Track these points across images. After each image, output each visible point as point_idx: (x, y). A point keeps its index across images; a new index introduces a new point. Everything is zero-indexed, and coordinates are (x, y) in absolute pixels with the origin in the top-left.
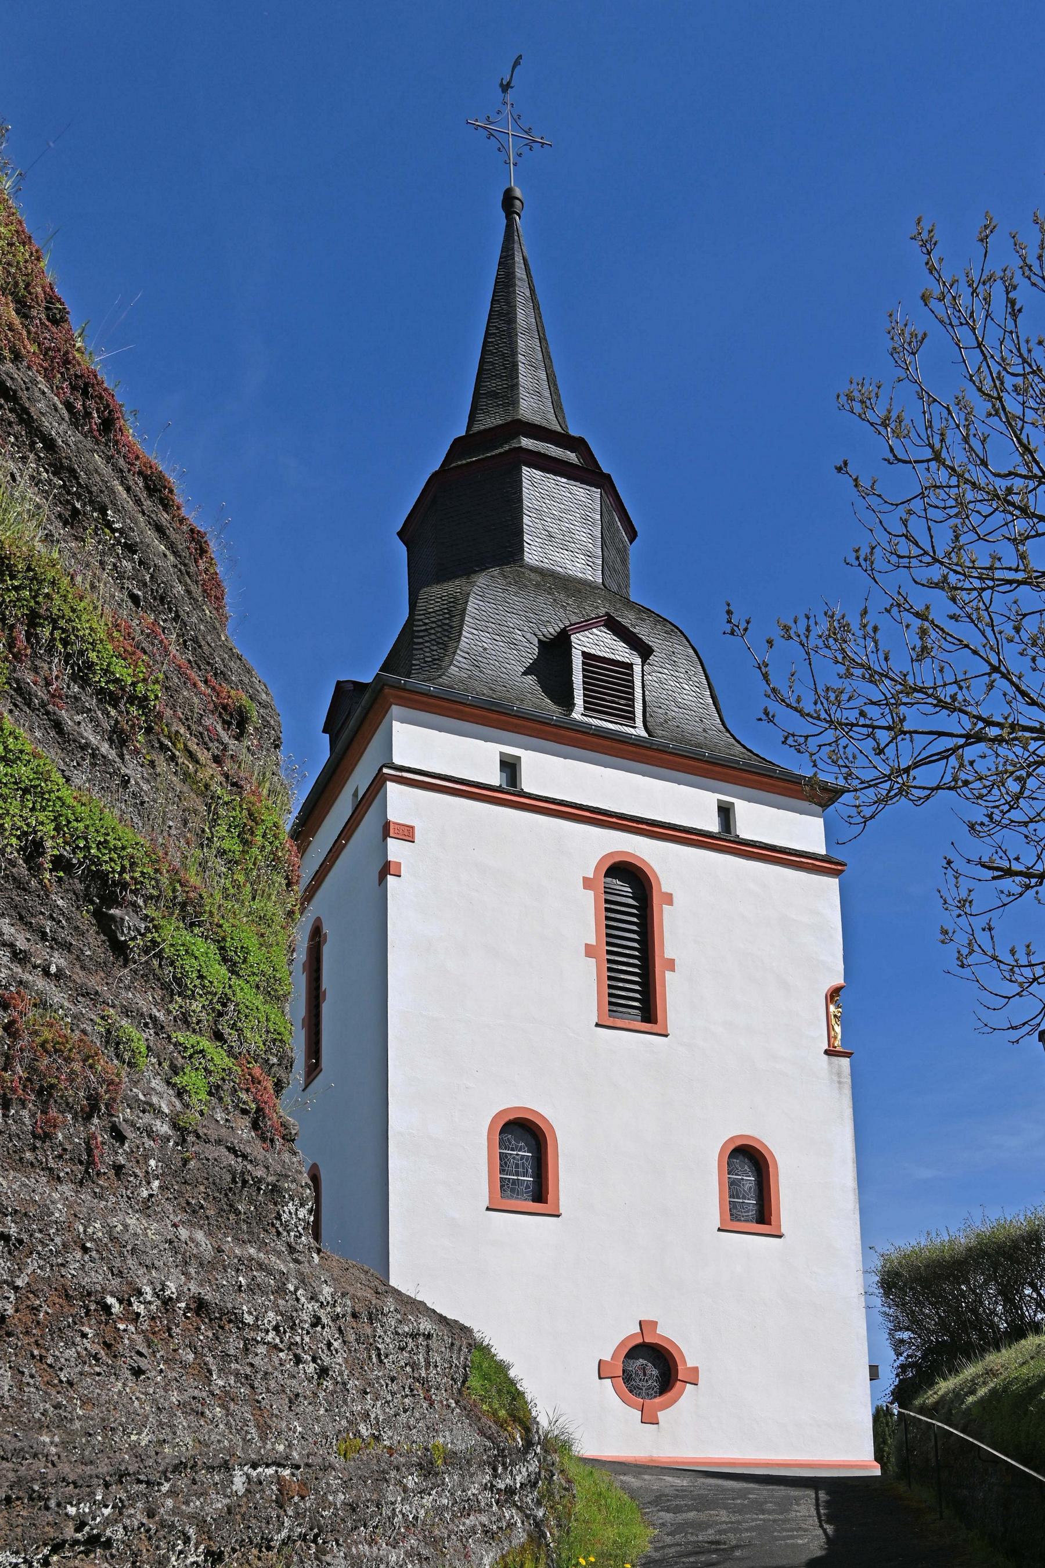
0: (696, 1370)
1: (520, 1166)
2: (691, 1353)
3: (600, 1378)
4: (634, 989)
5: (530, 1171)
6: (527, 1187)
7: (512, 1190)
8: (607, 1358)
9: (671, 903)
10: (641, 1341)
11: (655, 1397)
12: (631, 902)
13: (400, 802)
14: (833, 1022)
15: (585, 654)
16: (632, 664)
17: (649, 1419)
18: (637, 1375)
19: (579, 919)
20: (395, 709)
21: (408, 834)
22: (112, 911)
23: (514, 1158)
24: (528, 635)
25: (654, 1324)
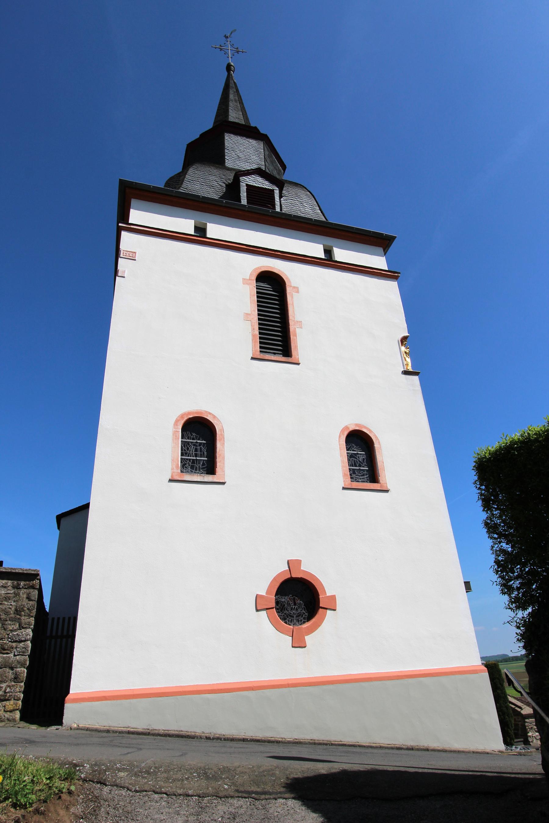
0: (333, 598)
1: (199, 450)
2: (329, 585)
3: (257, 610)
4: (275, 335)
5: (205, 453)
6: (203, 464)
7: (192, 467)
8: (263, 593)
9: (298, 292)
10: (289, 576)
11: (304, 622)
12: (272, 294)
13: (128, 240)
14: (405, 356)
15: (247, 185)
16: (273, 190)
17: (299, 644)
18: (289, 604)
19: (244, 302)
20: (134, 202)
21: (132, 257)
22: (530, 610)
23: (194, 445)
24: (221, 183)
25: (299, 562)
